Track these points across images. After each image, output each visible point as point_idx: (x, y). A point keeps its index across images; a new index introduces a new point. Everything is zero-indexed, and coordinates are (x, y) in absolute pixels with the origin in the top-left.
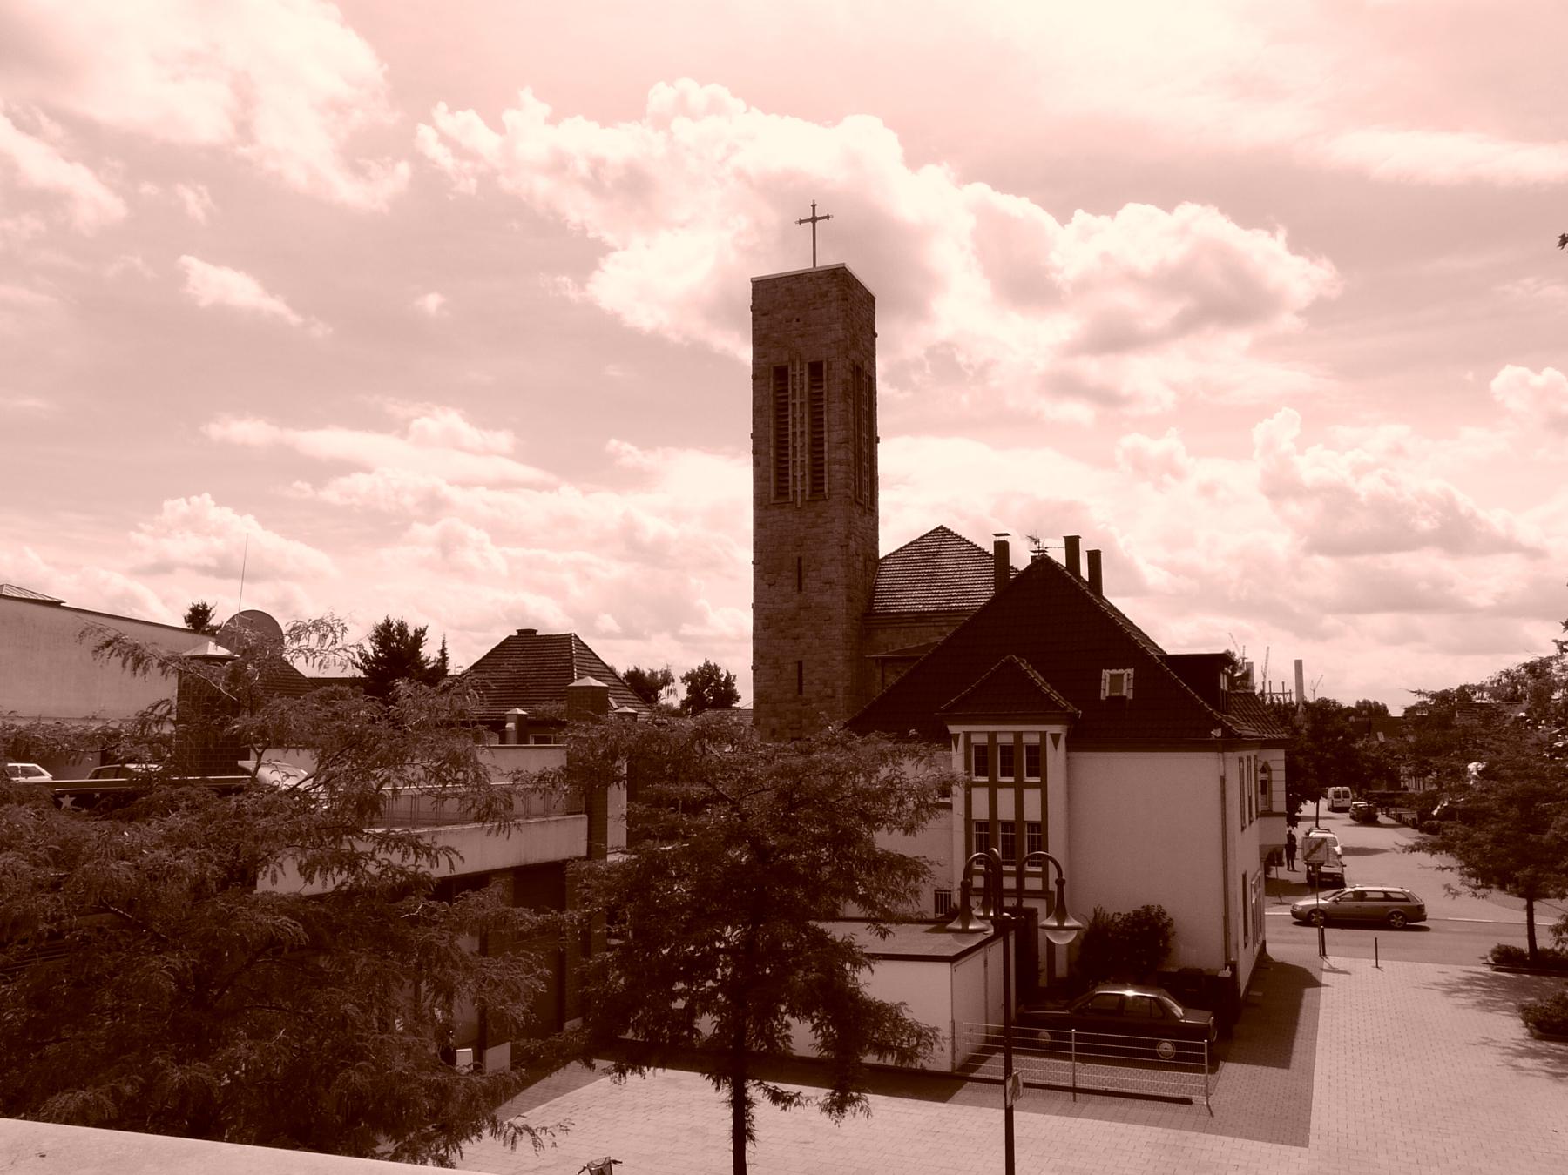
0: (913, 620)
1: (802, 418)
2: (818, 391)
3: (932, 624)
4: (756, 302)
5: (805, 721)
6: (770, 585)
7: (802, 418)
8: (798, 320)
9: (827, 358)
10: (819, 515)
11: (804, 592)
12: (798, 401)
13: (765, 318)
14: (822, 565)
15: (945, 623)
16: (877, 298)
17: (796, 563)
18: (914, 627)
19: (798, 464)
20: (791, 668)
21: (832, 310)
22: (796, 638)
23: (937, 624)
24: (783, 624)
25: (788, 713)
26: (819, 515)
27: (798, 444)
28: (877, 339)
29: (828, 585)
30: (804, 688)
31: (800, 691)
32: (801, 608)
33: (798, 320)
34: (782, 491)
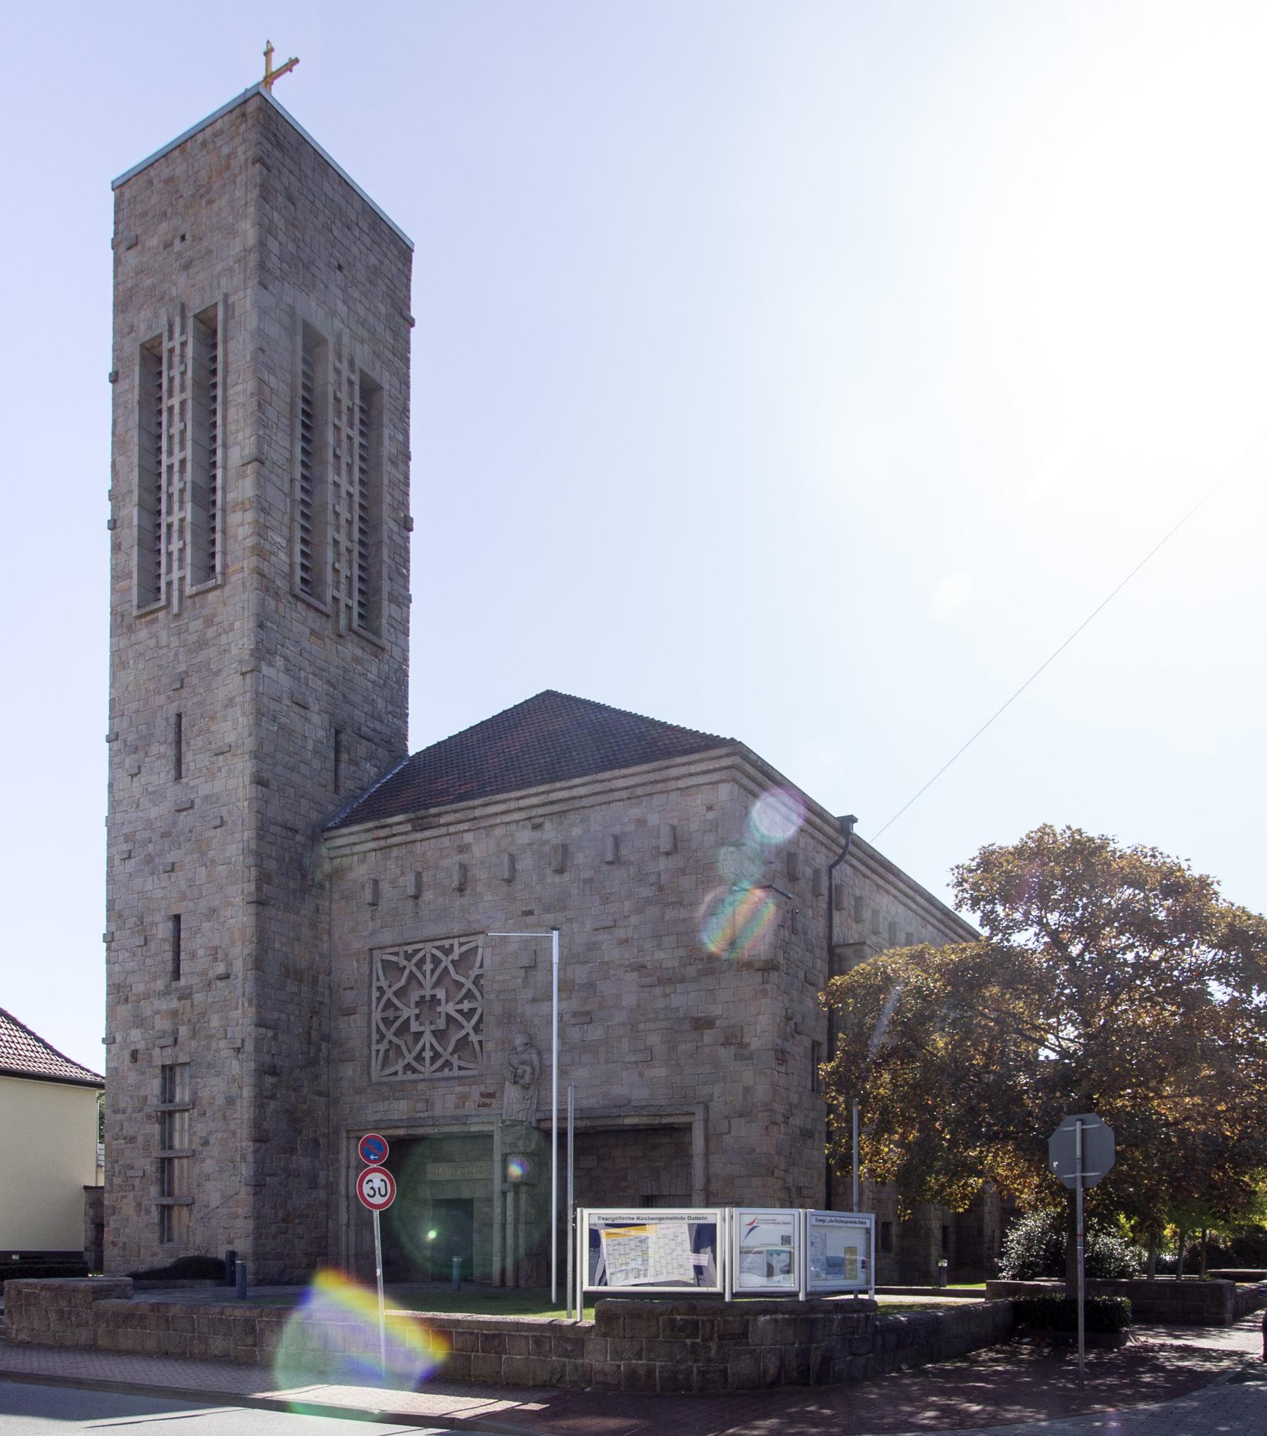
0: (408, 827)
1: (183, 432)
2: (752, 785)
3: (443, 830)
4: (121, 227)
5: (183, 1031)
6: (132, 776)
7: (183, 432)
8: (183, 238)
9: (226, 296)
10: (209, 622)
11: (184, 780)
12: (176, 402)
13: (132, 253)
14: (213, 718)
15: (465, 826)
16: (415, 249)
17: (173, 720)
18: (414, 842)
19: (176, 527)
20: (163, 930)
21: (1187, 1100)
22: (172, 869)
23: (452, 829)
24: (151, 846)
25: (157, 1017)
26: (209, 622)
27: (175, 489)
28: (412, 330)
29: (221, 757)
30: (185, 967)
31: (176, 975)
32: (179, 811)
33: (183, 238)
34: (151, 588)
